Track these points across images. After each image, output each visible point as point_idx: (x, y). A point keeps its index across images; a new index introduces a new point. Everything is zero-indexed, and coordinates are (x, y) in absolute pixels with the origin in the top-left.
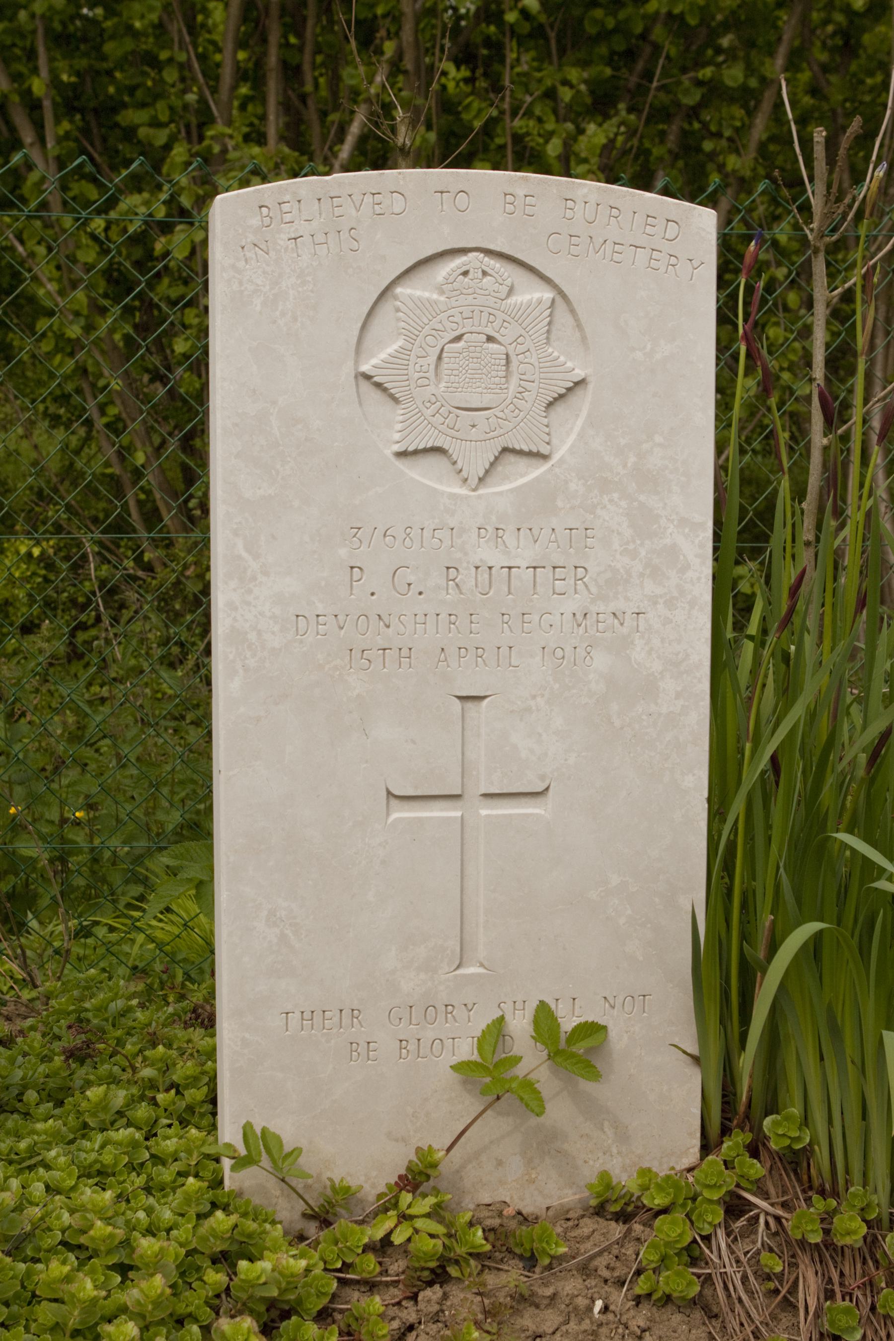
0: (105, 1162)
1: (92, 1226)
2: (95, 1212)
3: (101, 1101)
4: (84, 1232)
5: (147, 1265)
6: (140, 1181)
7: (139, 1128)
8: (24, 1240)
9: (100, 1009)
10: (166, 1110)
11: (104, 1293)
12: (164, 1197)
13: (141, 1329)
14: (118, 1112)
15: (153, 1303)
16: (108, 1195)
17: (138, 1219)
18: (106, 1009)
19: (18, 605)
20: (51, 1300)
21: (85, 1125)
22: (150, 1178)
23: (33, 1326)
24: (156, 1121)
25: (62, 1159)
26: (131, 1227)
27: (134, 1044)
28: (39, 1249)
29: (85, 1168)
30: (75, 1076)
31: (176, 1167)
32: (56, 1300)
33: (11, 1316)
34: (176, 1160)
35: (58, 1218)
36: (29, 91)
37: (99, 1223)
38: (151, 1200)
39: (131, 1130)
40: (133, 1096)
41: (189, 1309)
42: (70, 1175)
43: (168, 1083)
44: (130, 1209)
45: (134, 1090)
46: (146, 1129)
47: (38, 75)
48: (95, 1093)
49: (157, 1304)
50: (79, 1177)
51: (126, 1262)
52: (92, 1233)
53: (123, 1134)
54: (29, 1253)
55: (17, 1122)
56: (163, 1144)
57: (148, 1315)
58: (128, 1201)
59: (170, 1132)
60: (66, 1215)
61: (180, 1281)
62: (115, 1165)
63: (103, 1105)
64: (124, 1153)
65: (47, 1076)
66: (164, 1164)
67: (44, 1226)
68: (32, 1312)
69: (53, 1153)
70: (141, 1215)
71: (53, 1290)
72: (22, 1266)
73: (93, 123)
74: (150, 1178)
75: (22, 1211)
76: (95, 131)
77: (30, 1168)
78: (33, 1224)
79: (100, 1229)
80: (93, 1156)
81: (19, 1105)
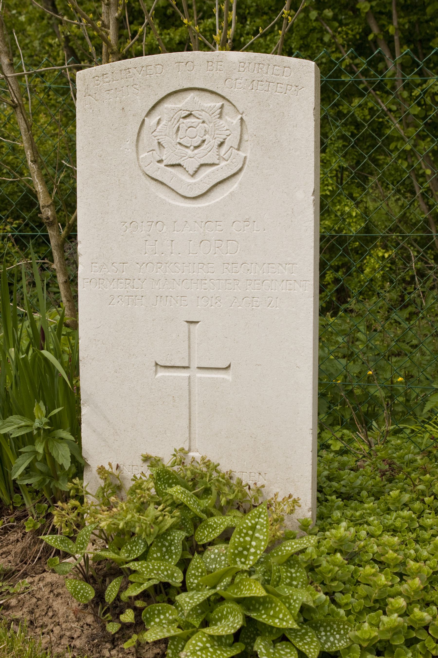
0: (396, 525)
1: (387, 553)
2: (389, 546)
3: (397, 497)
4: (382, 555)
5: (412, 573)
6: (414, 536)
7: (414, 513)
8: (355, 556)
9: (401, 457)
10: (429, 506)
11: (390, 583)
12: (424, 545)
13: (407, 604)
14: (404, 504)
15: (414, 591)
16: (396, 539)
17: (410, 554)
18: (403, 458)
19: (377, 281)
20: (365, 584)
21: (389, 509)
22: (418, 536)
23: (356, 595)
24: (423, 511)
25: (376, 522)
26: (406, 556)
27: (415, 474)
28: (361, 561)
29: (386, 527)
30: (386, 487)
31: (431, 532)
32: (368, 585)
33: (345, 589)
34: (432, 529)
35: (372, 547)
36: (387, 32)
37: (391, 552)
38: (418, 546)
39: (411, 512)
40: (413, 498)
41: (432, 599)
42: (379, 529)
43: (431, 493)
44: (407, 549)
45: (414, 496)
46: (418, 514)
47: (393, 25)
48: (394, 493)
49: (416, 592)
50: (383, 531)
51: (403, 572)
52: (387, 555)
53: (406, 513)
54: (357, 561)
55: (356, 504)
56: (426, 521)
57: (411, 597)
58: (406, 545)
59: (430, 516)
60: (375, 547)
61: (429, 586)
62: (402, 527)
63: (397, 500)
64: (406, 522)
65: (373, 486)
66: (426, 530)
67: (365, 550)
68: (356, 589)
69: (372, 519)
70: (412, 552)
71: (366, 579)
72: (352, 567)
73: (419, 47)
74: (418, 536)
75: (355, 543)
76: (420, 51)
77: (360, 524)
78: (359, 549)
79: (391, 554)
80: (390, 522)
81: (358, 497)
